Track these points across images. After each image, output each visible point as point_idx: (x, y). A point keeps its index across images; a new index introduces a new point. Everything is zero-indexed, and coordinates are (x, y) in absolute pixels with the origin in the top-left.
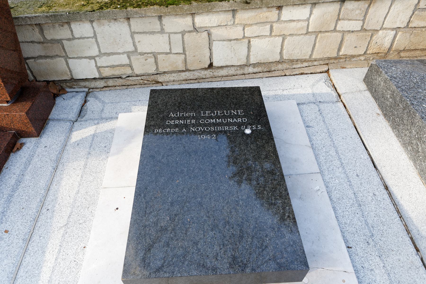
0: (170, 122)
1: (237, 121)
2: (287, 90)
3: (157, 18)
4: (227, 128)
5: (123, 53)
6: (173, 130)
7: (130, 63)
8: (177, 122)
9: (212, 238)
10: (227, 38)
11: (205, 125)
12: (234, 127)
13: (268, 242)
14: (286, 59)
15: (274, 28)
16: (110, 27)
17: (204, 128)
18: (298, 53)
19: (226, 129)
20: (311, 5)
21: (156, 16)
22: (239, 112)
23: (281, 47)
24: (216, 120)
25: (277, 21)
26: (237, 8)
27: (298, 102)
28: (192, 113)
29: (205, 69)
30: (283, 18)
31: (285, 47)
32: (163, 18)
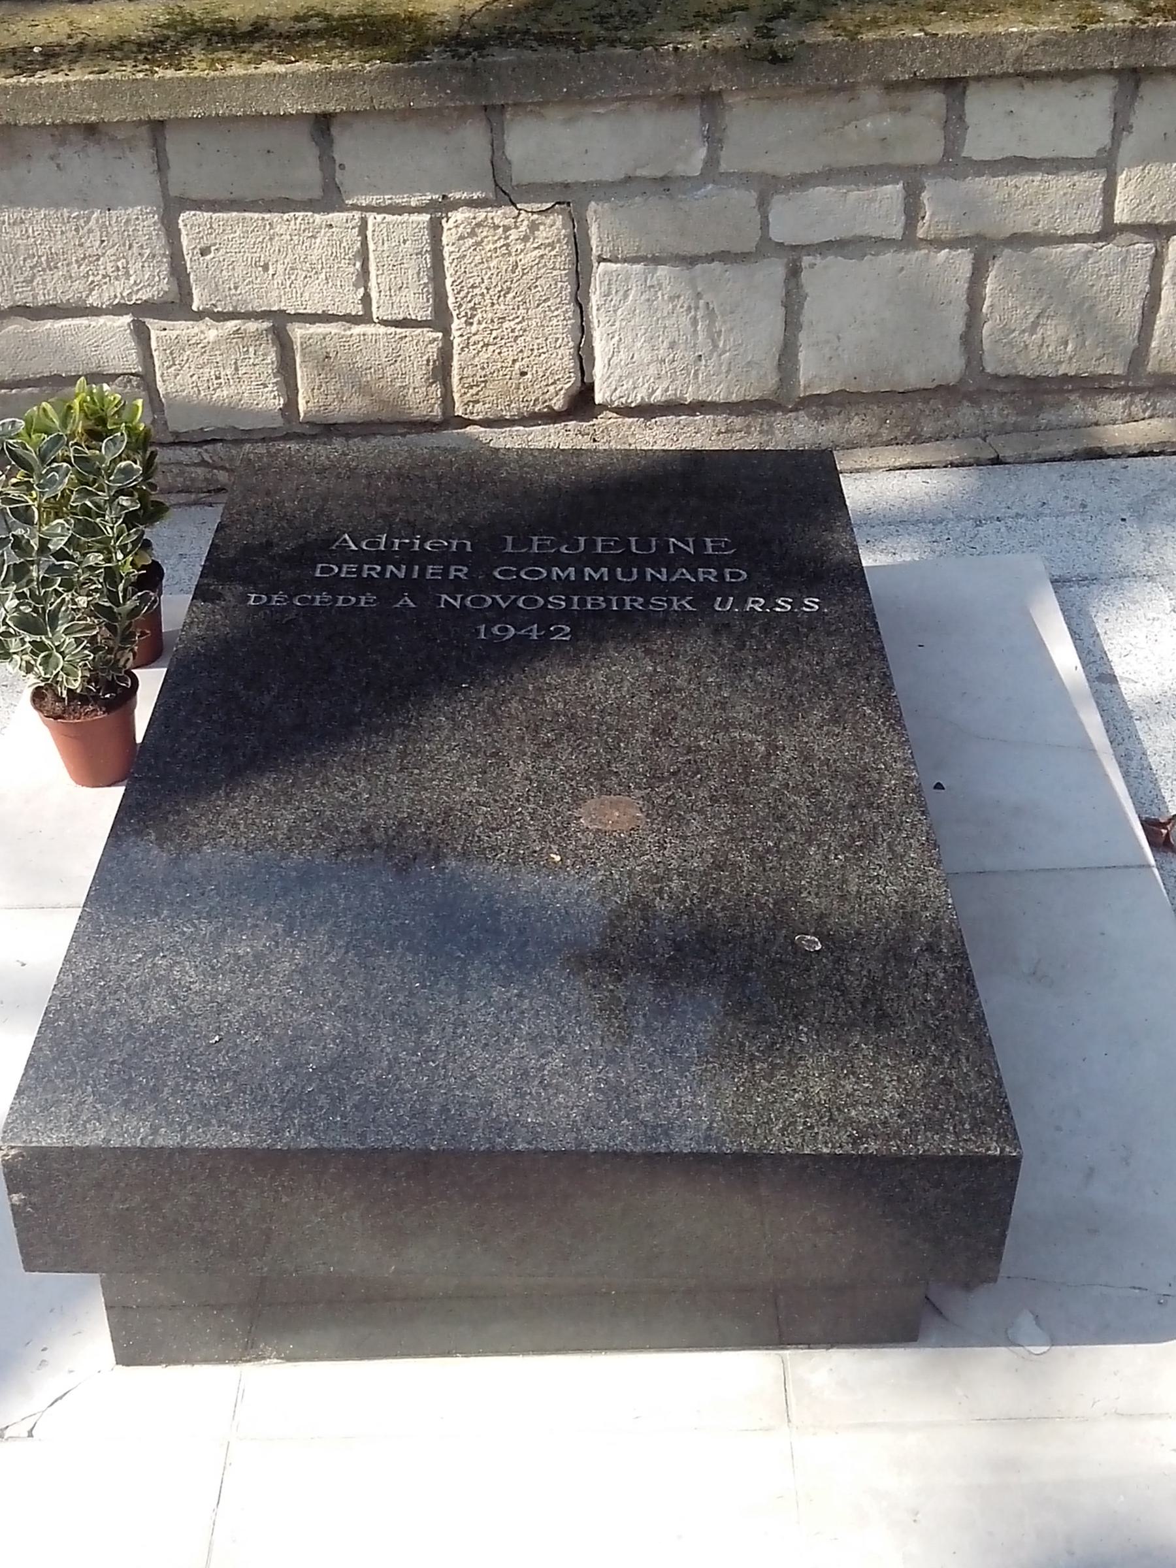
0: (336, 570)
1: (696, 577)
2: (998, 519)
3: (306, 128)
4: (636, 604)
5: (118, 309)
6: (346, 601)
7: (145, 367)
8: (370, 570)
9: (501, 1012)
10: (671, 250)
11: (520, 587)
12: (675, 599)
13: (804, 1039)
14: (996, 377)
15: (926, 202)
16: (58, 166)
17: (513, 597)
18: (1066, 344)
19: (632, 606)
20: (1112, 82)
21: (300, 115)
22: (709, 545)
23: (966, 307)
24: (583, 572)
25: (941, 164)
26: (723, 86)
27: (1057, 573)
28: (455, 543)
29: (553, 417)
30: (976, 147)
31: (987, 303)
32: (335, 131)
